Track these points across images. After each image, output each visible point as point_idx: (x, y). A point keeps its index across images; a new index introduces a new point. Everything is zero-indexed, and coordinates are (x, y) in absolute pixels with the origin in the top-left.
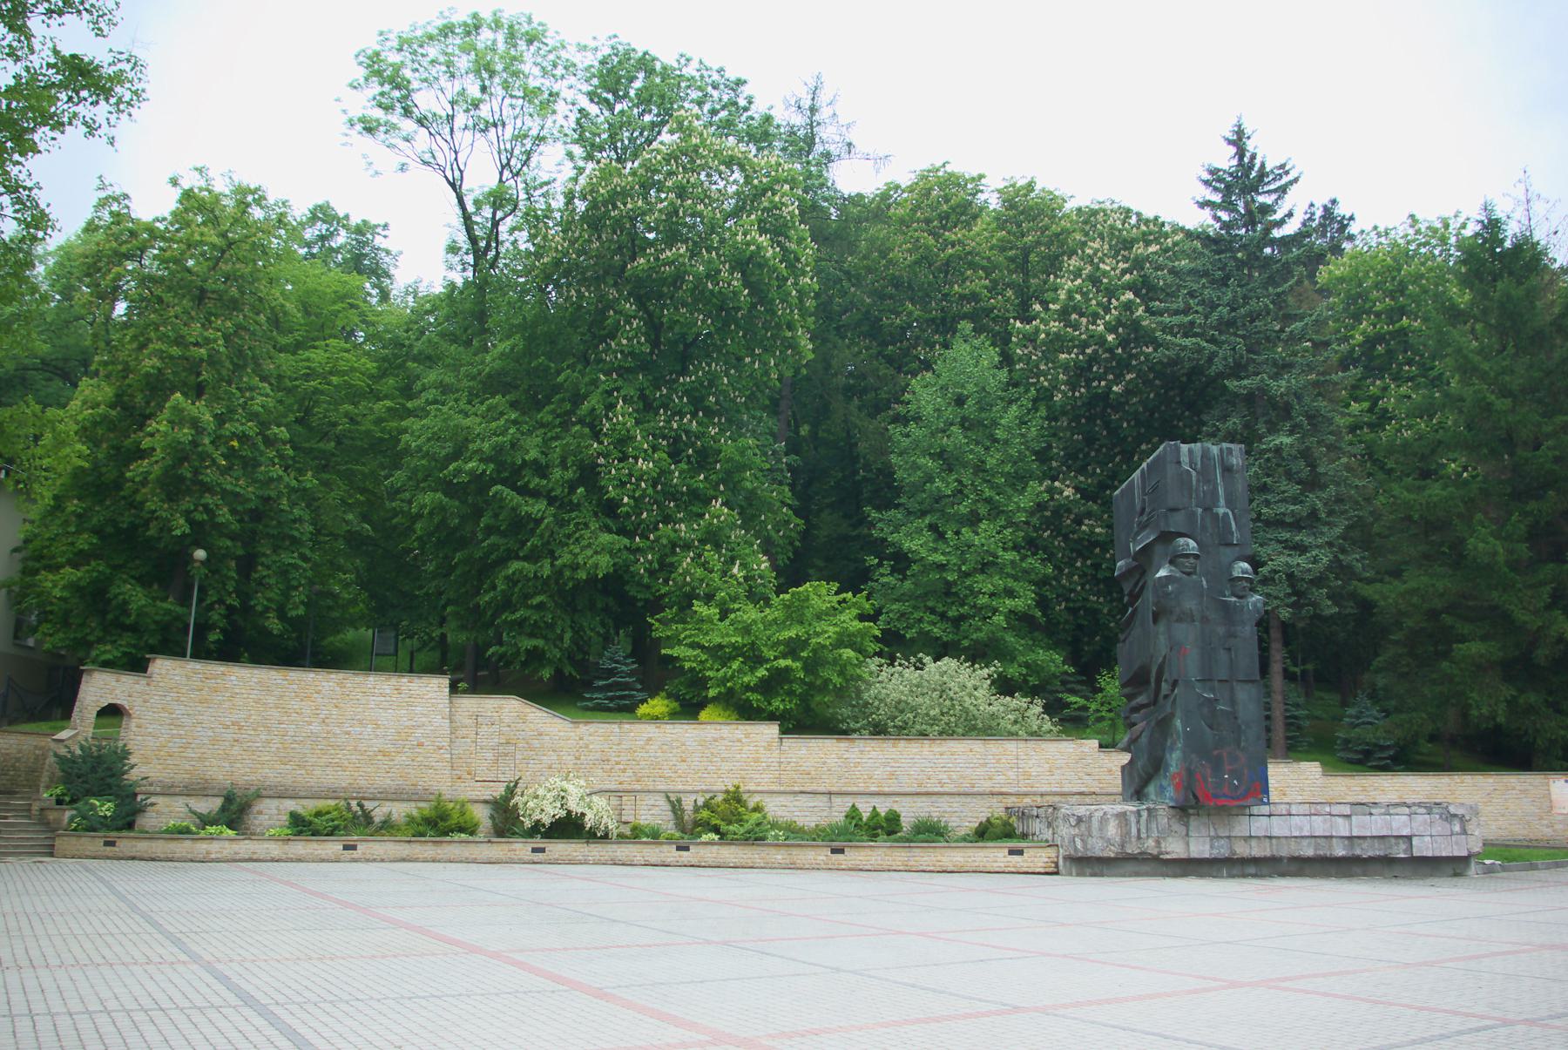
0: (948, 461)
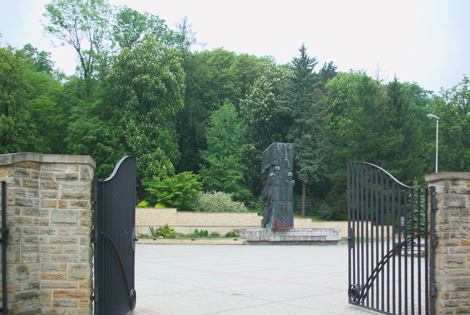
0: (221, 138)
